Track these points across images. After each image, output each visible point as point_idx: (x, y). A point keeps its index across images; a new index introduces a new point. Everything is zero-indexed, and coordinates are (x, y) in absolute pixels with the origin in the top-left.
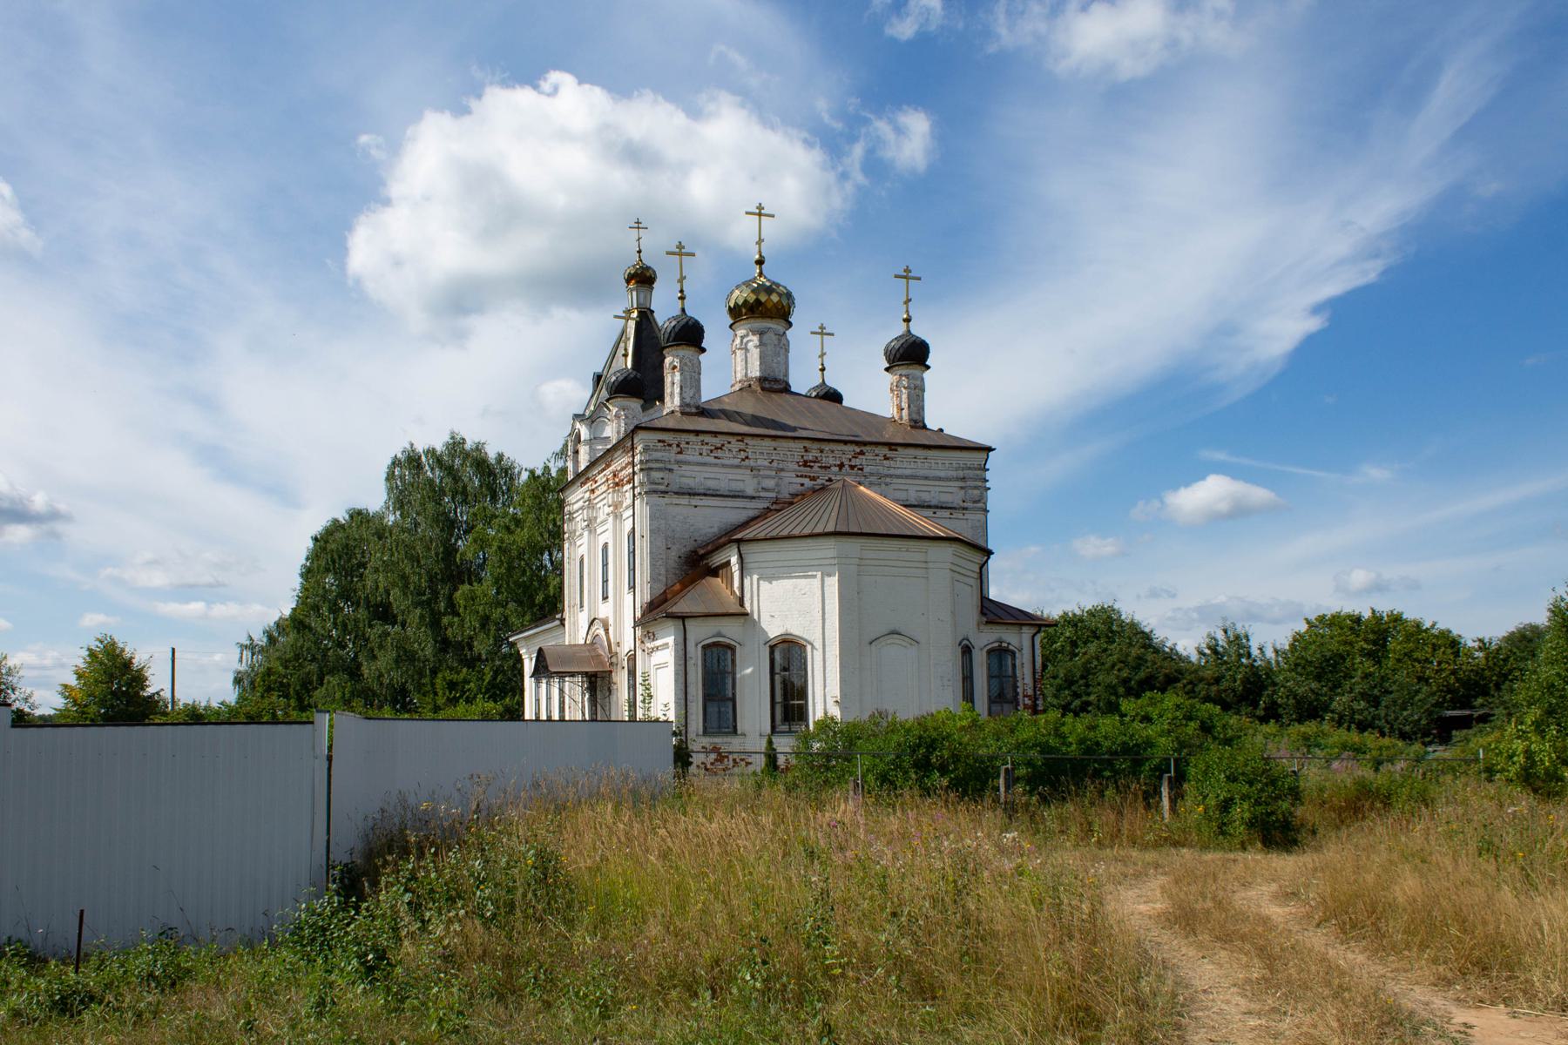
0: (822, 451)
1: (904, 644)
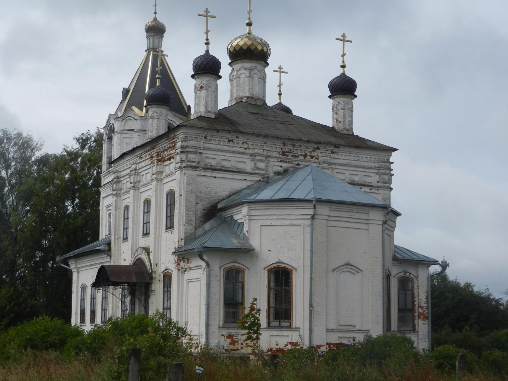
0: (294, 146)
1: (354, 272)
